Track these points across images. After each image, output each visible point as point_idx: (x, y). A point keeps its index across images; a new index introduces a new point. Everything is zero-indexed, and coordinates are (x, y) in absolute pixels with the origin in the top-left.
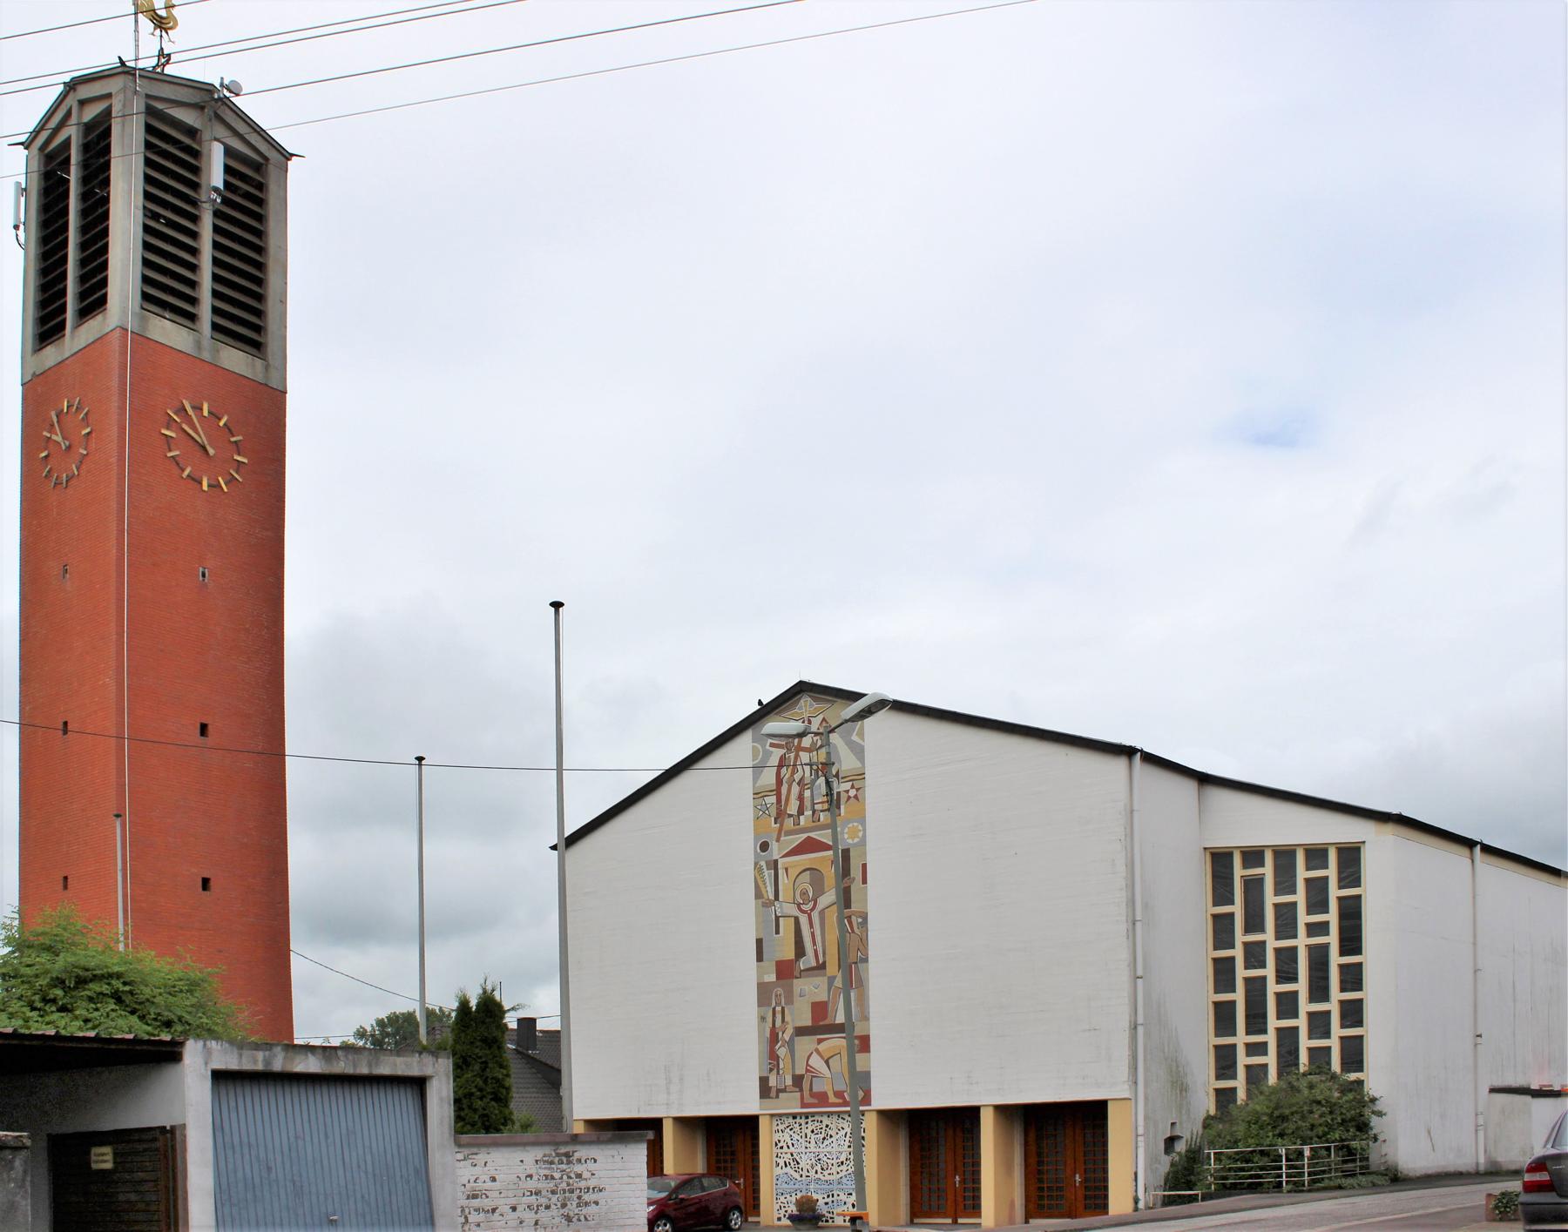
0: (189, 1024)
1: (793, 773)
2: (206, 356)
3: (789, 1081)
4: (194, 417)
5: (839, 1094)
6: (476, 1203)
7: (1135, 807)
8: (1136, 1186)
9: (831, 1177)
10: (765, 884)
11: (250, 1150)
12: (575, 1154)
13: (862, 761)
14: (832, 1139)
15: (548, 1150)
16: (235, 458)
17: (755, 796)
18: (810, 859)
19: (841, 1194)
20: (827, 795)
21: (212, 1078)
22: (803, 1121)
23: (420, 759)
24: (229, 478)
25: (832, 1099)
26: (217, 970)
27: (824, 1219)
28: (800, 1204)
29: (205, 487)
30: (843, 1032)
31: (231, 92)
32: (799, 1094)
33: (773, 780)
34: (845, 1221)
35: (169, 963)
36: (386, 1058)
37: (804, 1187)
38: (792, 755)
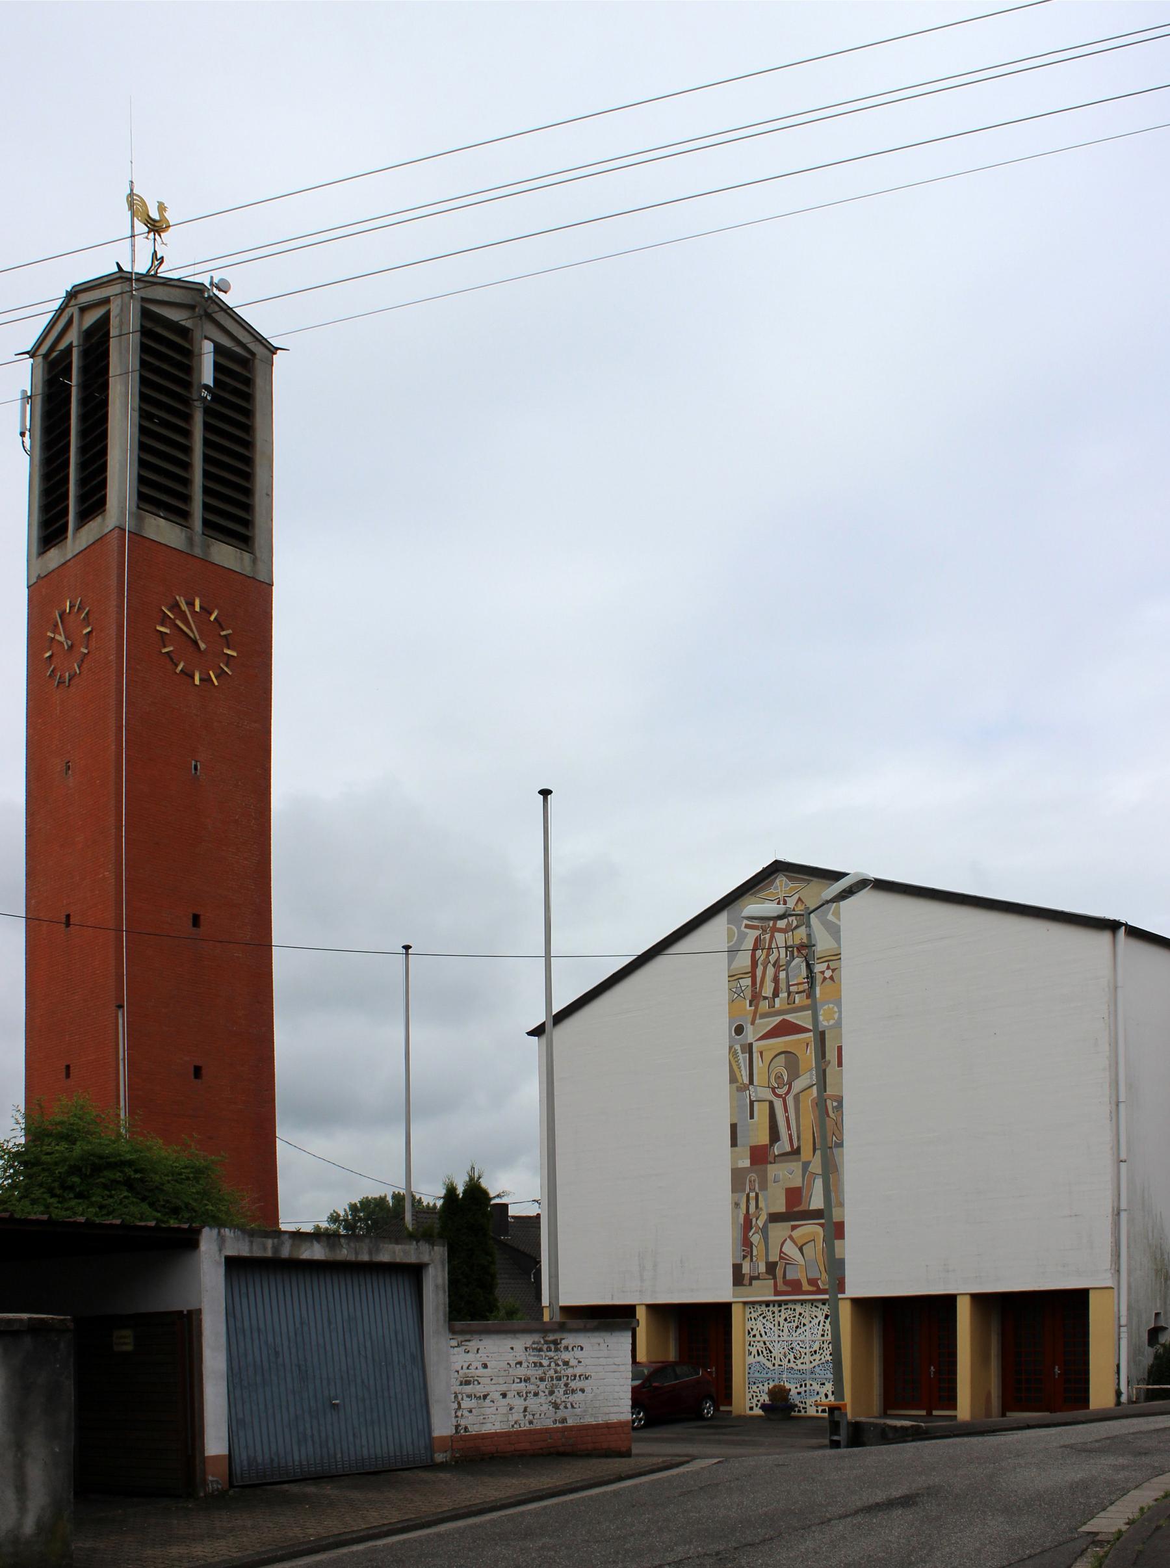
0: (195, 1211)
1: (768, 955)
2: (198, 551)
3: (762, 1268)
4: (188, 613)
5: (813, 1282)
6: (468, 1389)
7: (1119, 984)
8: (1119, 1379)
9: (804, 1367)
10: (739, 1068)
11: (259, 1336)
12: (563, 1342)
13: (838, 939)
14: (805, 1328)
15: (536, 1337)
16: (225, 651)
17: (731, 979)
18: (785, 1042)
19: (814, 1384)
20: (807, 978)
21: (225, 1265)
22: (776, 1309)
23: (407, 948)
24: (219, 671)
25: (806, 1286)
26: (220, 1158)
27: (797, 1409)
28: (771, 1393)
29: (197, 682)
30: (823, 1219)
31: (220, 290)
32: (773, 1281)
33: (748, 962)
34: (817, 1411)
35: (176, 1152)
36: (387, 1245)
37: (777, 1376)
38: (768, 936)
